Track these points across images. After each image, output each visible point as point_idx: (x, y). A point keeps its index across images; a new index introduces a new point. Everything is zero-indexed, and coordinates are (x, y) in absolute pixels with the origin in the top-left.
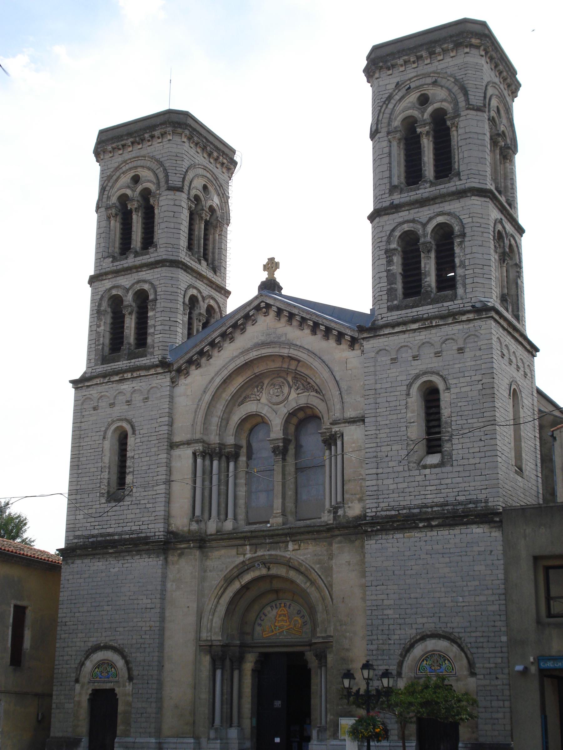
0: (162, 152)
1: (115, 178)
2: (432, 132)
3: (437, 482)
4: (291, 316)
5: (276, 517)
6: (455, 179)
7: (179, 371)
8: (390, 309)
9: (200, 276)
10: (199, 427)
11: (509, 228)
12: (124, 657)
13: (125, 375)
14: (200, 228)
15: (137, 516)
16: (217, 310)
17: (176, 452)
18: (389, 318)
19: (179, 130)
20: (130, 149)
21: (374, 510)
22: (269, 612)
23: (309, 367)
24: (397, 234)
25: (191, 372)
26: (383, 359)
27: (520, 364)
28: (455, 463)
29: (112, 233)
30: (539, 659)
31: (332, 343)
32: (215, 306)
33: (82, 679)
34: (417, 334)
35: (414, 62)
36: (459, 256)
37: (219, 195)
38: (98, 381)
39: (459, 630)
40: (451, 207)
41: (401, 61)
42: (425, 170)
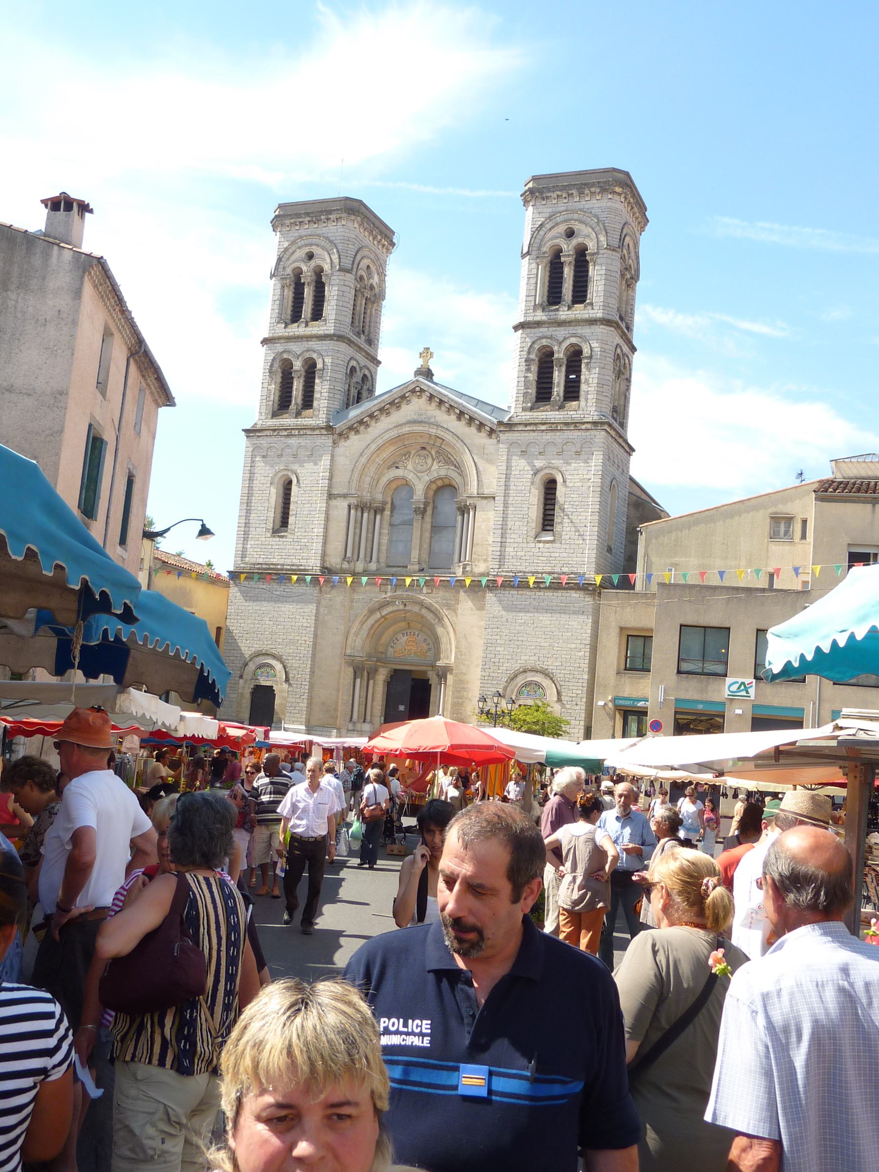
0: (336, 235)
1: (291, 251)
2: (574, 262)
3: (548, 554)
4: (441, 402)
5: (413, 564)
6: (589, 307)
7: (340, 435)
8: (524, 409)
9: (360, 349)
10: (354, 485)
11: (626, 349)
12: (282, 663)
13: (293, 432)
14: (361, 304)
15: (298, 551)
16: (370, 378)
17: (334, 503)
18: (523, 417)
19: (353, 217)
20: (306, 226)
21: (496, 570)
22: (401, 638)
23: (452, 447)
24: (537, 346)
25: (350, 437)
26: (515, 450)
27: (620, 464)
28: (563, 541)
29: (285, 301)
30: (614, 700)
31: (473, 430)
32: (369, 375)
33: (245, 676)
34: (544, 434)
35: (565, 198)
36: (585, 374)
37: (378, 274)
38: (268, 433)
39: (552, 667)
40: (583, 331)
41: (554, 195)
42: (565, 295)
